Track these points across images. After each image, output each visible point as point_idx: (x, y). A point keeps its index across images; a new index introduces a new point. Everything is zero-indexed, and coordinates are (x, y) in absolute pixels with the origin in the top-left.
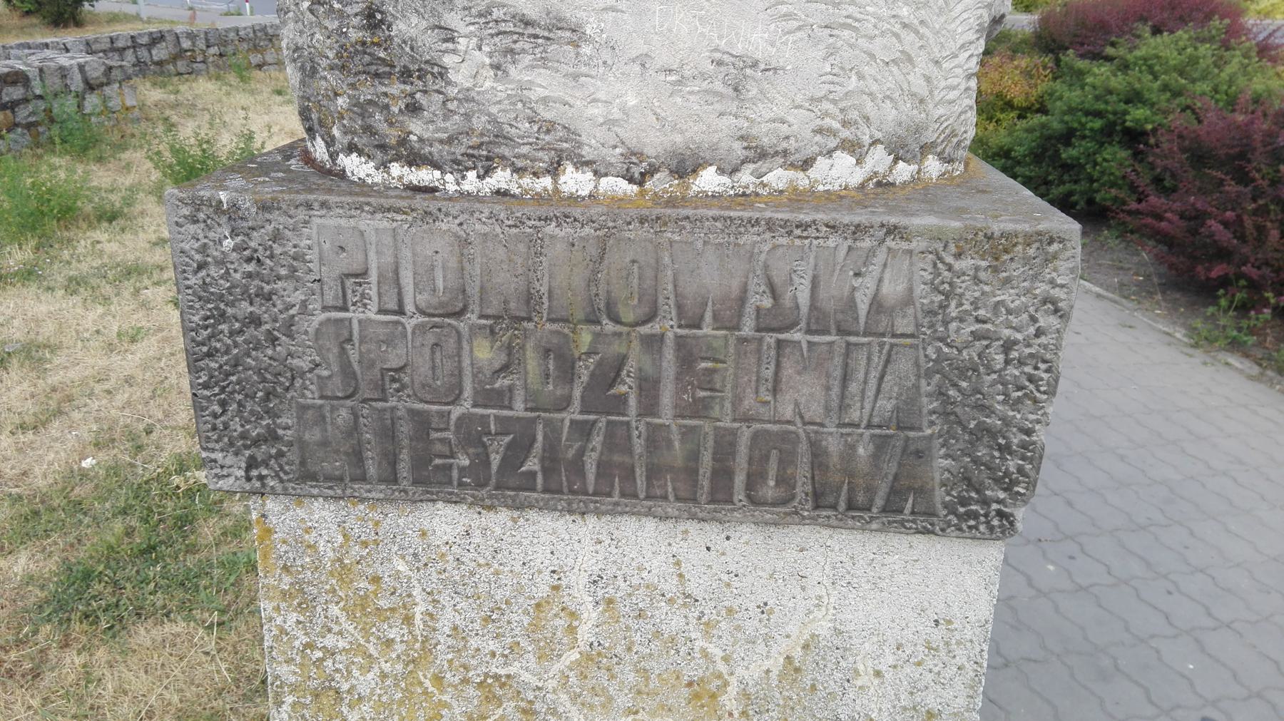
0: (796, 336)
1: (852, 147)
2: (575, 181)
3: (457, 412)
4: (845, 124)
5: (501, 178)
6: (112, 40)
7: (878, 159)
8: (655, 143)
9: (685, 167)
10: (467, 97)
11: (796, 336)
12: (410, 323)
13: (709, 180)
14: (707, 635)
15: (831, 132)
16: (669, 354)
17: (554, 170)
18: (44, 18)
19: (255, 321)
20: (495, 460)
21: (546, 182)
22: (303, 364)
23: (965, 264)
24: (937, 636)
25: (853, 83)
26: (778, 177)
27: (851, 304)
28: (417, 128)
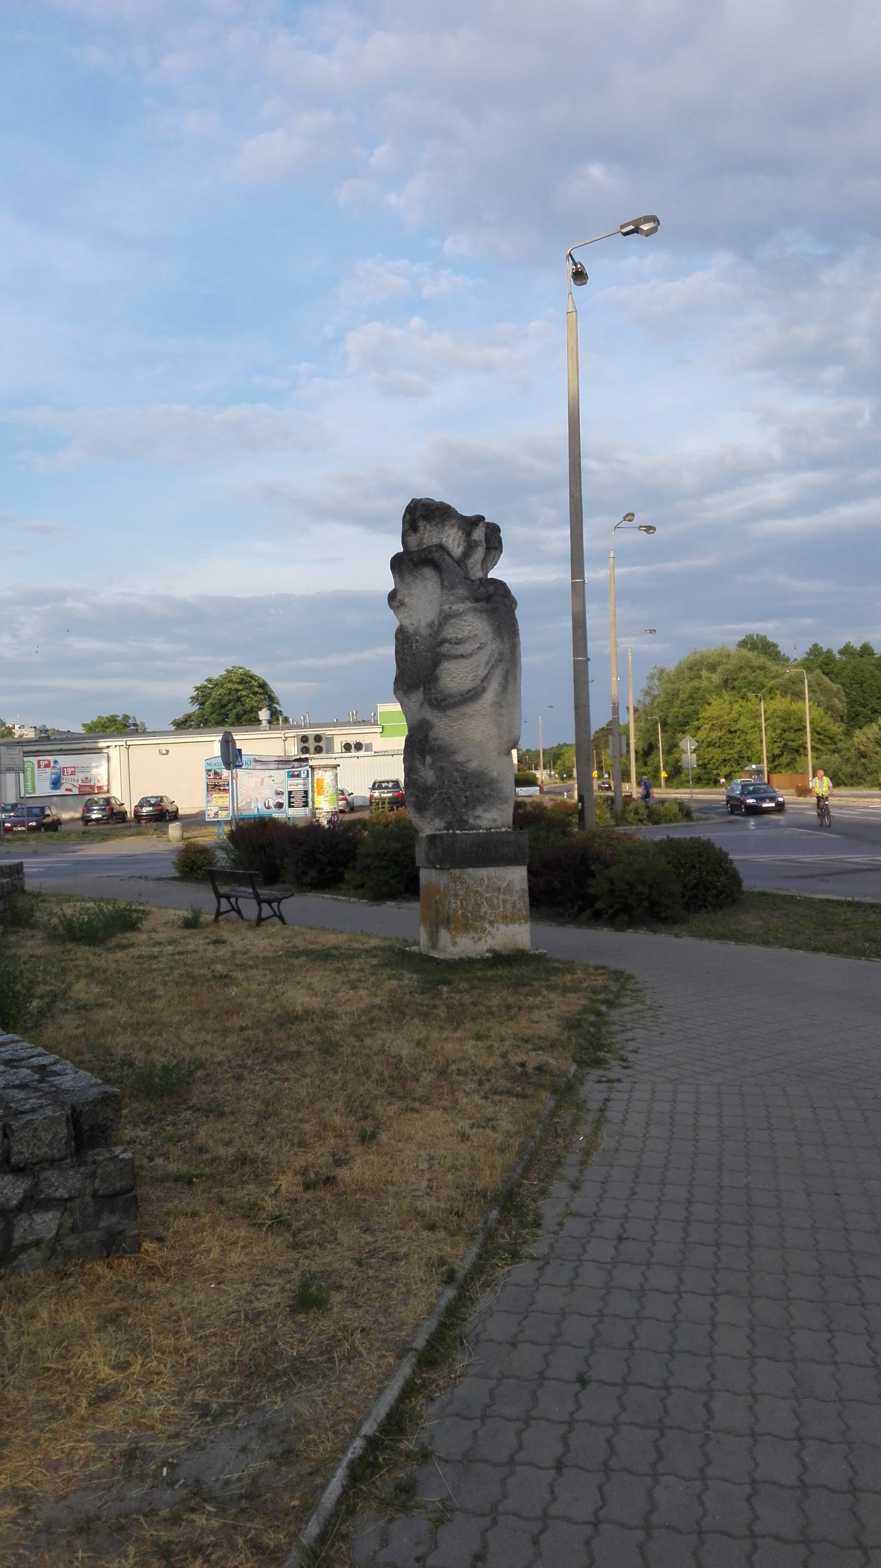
2: (481, 831)
9: (490, 829)
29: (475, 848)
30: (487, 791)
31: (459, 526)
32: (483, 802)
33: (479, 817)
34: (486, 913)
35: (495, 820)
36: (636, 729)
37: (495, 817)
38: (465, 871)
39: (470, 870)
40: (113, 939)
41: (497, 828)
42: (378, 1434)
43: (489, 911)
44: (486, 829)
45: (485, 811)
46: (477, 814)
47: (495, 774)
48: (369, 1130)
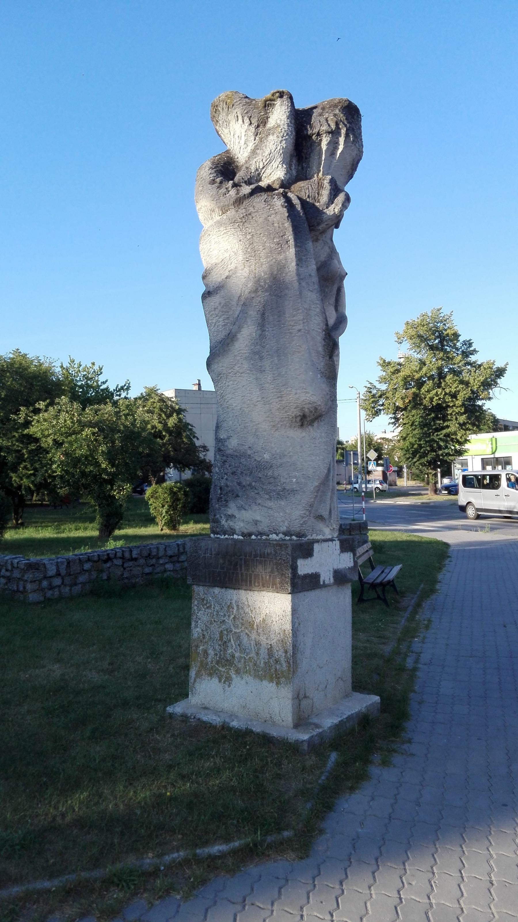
0: (258, 558)
1: (276, 533)
2: (236, 537)
3: (218, 570)
4: (274, 530)
5: (227, 536)
6: (62, 508)
7: (281, 536)
8: (246, 531)
9: (250, 535)
10: (223, 525)
11: (258, 558)
12: (213, 556)
13: (253, 537)
14: (252, 613)
15: (271, 531)
16: (243, 561)
17: (233, 535)
18: (134, 521)
19: (195, 556)
20: (222, 578)
21: (232, 537)
22: (200, 563)
23: (277, 548)
24: (284, 613)
25: (274, 524)
26: (264, 537)
27: (264, 553)
28: (218, 529)
29: (221, 561)
30: (246, 480)
31: (485, 415)
32: (237, 496)
33: (231, 517)
34: (233, 656)
35: (256, 522)
36: (470, 549)
37: (258, 518)
38: (211, 590)
39: (217, 590)
40: (27, 530)
41: (261, 534)
42: (305, 747)
43: (237, 655)
44: (243, 535)
45: (241, 508)
46: (230, 512)
47: (267, 456)
48: (396, 469)
